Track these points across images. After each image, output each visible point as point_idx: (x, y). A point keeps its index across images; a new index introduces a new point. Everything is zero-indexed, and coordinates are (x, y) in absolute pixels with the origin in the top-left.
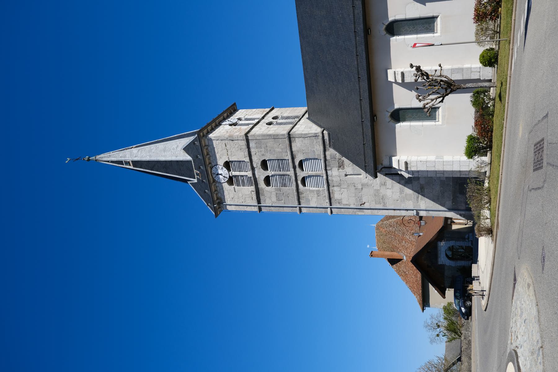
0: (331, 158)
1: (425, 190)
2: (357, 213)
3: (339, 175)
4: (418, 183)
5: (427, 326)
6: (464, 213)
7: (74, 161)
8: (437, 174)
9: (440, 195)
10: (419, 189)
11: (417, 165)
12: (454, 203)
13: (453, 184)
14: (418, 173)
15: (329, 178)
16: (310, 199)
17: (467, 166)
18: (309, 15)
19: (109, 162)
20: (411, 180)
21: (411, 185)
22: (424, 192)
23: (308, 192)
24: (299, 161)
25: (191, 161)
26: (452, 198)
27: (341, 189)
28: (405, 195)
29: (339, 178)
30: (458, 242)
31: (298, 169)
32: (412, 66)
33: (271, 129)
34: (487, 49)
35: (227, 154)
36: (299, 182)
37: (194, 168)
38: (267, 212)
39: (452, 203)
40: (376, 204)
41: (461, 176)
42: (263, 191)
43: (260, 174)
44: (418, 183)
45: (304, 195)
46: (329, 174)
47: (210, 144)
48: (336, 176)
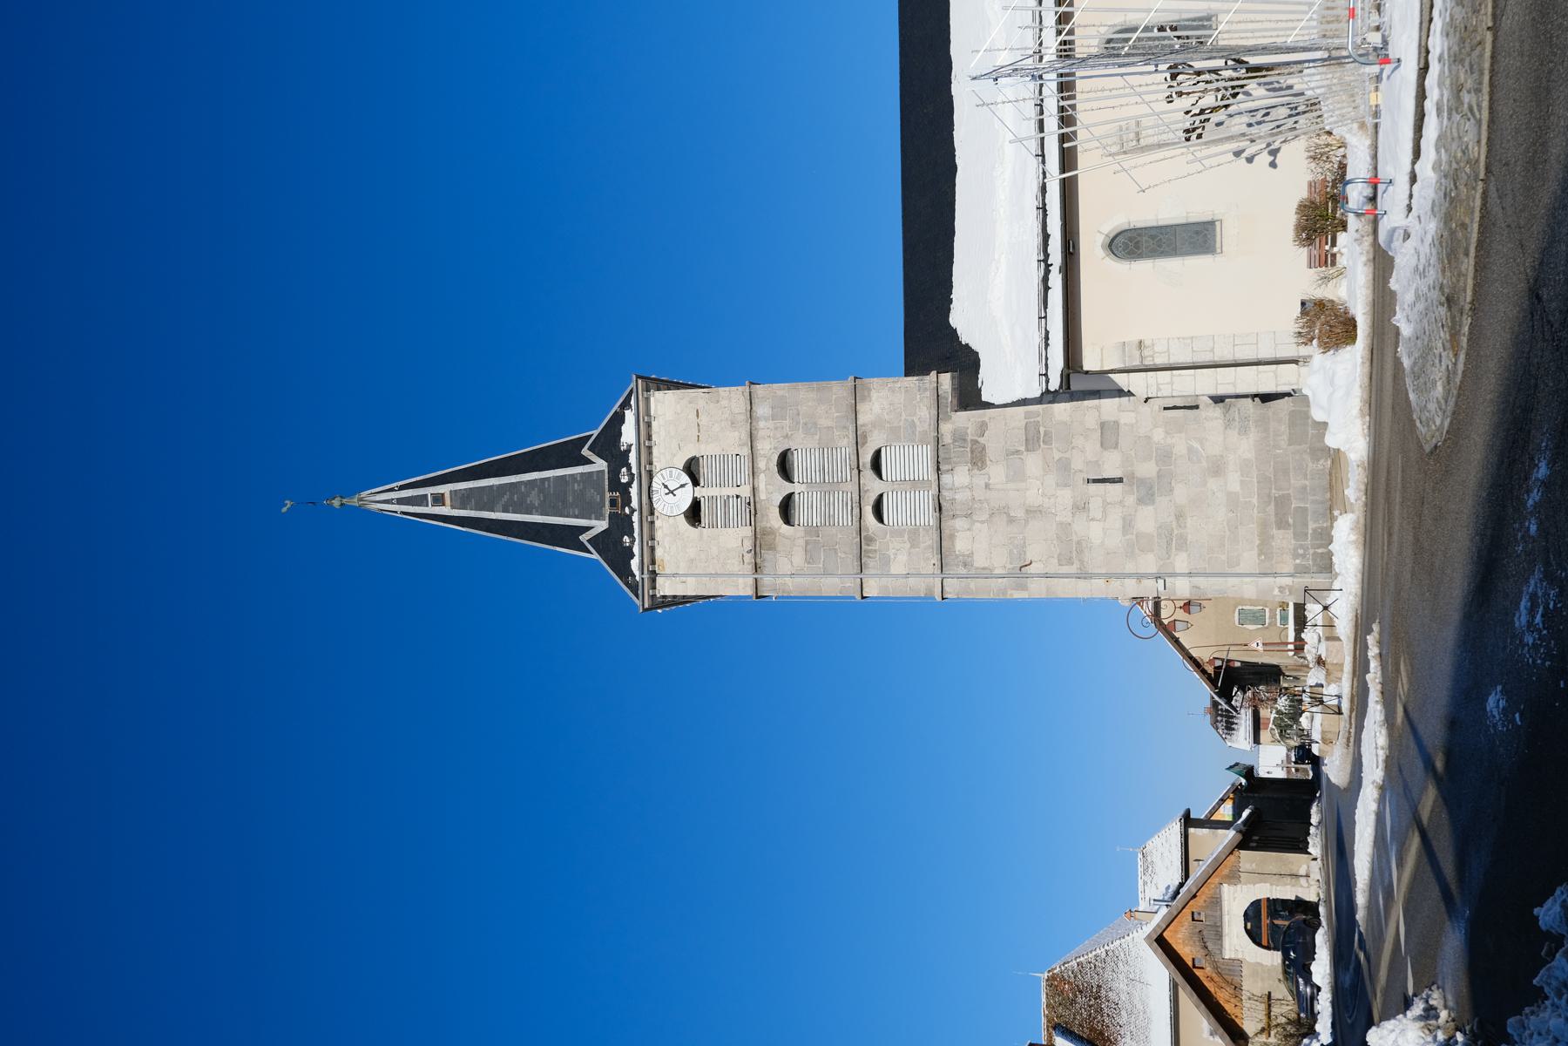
0: (955, 441)
1: (1189, 519)
2: (1009, 592)
4: (1171, 501)
6: (1291, 584)
9: (1228, 533)
10: (1173, 518)
11: (1168, 349)
13: (1259, 502)
14: (1172, 385)
15: (944, 493)
16: (892, 557)
20: (1153, 495)
22: (1185, 527)
24: (874, 450)
26: (1258, 542)
28: (1137, 536)
29: (969, 494)
30: (1278, 888)
31: (868, 473)
35: (699, 432)
36: (868, 510)
37: (607, 487)
39: (1259, 555)
40: (1060, 565)
44: (1171, 501)
46: (946, 484)
47: (659, 413)
48: (962, 487)
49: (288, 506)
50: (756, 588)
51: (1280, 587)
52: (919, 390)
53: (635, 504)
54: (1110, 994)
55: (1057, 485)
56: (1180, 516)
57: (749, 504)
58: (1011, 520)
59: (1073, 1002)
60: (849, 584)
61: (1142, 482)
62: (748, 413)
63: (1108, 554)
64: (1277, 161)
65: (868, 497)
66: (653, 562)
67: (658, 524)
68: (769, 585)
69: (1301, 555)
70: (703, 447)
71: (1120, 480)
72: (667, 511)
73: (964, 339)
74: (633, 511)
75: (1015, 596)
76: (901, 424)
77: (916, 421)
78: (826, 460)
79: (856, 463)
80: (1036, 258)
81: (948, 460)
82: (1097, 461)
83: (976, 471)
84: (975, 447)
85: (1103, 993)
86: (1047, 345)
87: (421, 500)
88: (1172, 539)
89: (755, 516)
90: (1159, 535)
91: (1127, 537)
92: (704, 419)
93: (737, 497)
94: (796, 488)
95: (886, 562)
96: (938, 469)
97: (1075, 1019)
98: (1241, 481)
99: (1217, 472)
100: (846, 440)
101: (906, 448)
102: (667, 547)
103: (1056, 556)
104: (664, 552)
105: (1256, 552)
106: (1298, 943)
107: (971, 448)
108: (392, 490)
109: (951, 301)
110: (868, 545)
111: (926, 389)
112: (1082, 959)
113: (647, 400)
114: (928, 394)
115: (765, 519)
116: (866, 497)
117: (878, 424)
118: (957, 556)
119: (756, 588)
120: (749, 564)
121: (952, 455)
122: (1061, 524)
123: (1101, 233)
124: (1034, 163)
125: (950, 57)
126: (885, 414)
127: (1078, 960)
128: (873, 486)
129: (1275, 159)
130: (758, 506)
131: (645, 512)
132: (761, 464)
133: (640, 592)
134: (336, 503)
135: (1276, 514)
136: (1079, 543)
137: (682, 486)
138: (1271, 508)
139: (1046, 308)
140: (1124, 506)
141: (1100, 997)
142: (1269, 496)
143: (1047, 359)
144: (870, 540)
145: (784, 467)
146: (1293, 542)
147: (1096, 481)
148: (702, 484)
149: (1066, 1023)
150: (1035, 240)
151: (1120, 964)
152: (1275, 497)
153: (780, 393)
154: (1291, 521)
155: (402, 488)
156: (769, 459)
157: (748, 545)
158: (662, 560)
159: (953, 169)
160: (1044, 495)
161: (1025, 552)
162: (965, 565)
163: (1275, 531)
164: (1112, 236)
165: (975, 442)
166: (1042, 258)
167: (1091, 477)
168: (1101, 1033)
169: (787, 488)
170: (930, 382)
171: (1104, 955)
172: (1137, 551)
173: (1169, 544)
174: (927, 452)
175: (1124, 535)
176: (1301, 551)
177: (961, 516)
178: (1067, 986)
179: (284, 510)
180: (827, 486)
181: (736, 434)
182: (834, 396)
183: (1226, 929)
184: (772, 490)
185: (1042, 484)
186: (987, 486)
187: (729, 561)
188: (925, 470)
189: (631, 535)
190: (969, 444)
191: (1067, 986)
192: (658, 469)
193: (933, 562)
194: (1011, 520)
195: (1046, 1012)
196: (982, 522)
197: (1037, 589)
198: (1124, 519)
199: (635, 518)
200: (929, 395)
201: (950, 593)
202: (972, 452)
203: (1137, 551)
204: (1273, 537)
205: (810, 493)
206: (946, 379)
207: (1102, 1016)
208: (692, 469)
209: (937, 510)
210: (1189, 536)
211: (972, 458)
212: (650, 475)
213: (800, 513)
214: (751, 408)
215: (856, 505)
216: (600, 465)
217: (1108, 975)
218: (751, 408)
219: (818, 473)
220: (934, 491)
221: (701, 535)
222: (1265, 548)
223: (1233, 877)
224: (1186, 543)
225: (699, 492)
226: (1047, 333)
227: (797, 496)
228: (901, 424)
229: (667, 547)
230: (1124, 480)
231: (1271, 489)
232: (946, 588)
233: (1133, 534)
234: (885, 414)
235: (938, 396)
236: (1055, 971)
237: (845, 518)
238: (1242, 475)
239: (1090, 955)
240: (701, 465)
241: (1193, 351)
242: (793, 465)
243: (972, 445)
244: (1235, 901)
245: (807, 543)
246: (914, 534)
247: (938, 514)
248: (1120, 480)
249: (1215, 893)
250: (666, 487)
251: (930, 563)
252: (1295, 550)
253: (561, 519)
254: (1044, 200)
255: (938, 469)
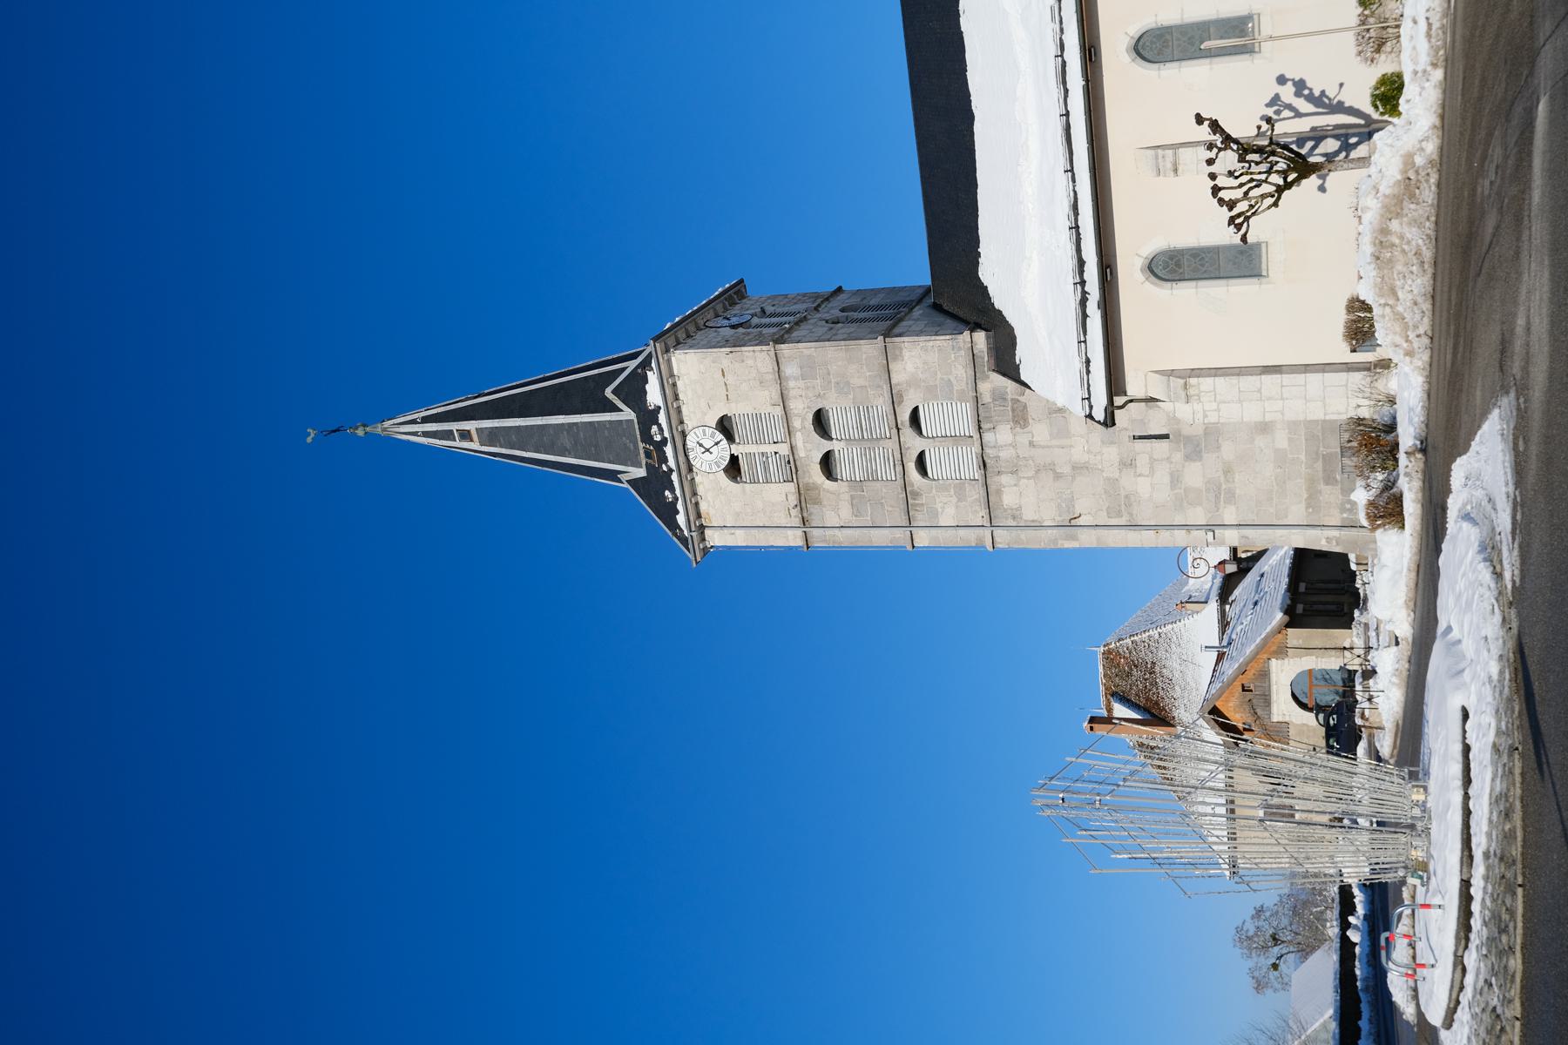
0: (994, 400)
1: (1237, 475)
2: (1060, 542)
3: (1014, 444)
4: (1218, 457)
5: (1246, 940)
7: (326, 435)
8: (1267, 414)
12: (1311, 510)
15: (987, 450)
16: (940, 510)
17: (1341, 386)
18: (939, 35)
19: (418, 436)
20: (1200, 451)
21: (1199, 464)
22: (1234, 481)
23: (934, 491)
25: (633, 420)
26: (1305, 496)
27: (1019, 480)
28: (1185, 490)
30: (1323, 660)
31: (908, 432)
32: (1199, 120)
33: (840, 331)
34: (1253, 915)
38: (825, 547)
39: (1307, 508)
40: (1109, 517)
41: (1328, 418)
42: (817, 492)
43: (809, 446)
45: (922, 500)
48: (1005, 446)
49: (312, 435)
50: (807, 540)
51: (1328, 538)
52: (953, 349)
53: (672, 463)
54: (1164, 671)
55: (1103, 442)
56: (1228, 471)
57: (789, 462)
58: (1058, 476)
59: (1129, 674)
60: (899, 535)
61: (1188, 440)
62: (777, 374)
63: (1157, 507)
64: (1326, 185)
65: (910, 454)
66: (699, 516)
67: (698, 479)
68: (819, 538)
69: (1349, 509)
70: (733, 405)
71: (1166, 437)
72: (705, 468)
73: (997, 306)
74: (671, 471)
75: (1066, 546)
76: (938, 382)
77: (952, 380)
78: (862, 417)
79: (894, 424)
80: (1072, 281)
81: (989, 419)
82: (1142, 420)
83: (1018, 429)
84: (1015, 406)
85: (1157, 669)
86: (1088, 372)
87: (448, 435)
88: (1220, 493)
89: (796, 474)
90: (1208, 490)
91: (1176, 491)
92: (730, 379)
93: (776, 453)
94: (835, 446)
95: (934, 514)
96: (980, 428)
97: (1131, 689)
98: (1289, 438)
99: (1265, 429)
100: (881, 399)
101: (945, 405)
102: (711, 501)
103: (1104, 508)
104: (709, 506)
105: (1303, 505)
106: (1342, 731)
107: (1012, 407)
108: (413, 422)
109: (979, 255)
110: (915, 499)
111: (960, 349)
112: (1136, 638)
113: (669, 361)
114: (963, 353)
115: (807, 475)
116: (908, 454)
117: (914, 382)
118: (1005, 510)
119: (807, 540)
120: (795, 517)
121: (993, 414)
122: (1108, 479)
123: (1139, 256)
124: (1063, 180)
125: (978, 237)
126: (919, 373)
127: (1132, 639)
128: (914, 444)
129: (1324, 182)
130: (798, 463)
131: (684, 471)
132: (796, 423)
133: (690, 546)
134: (360, 432)
135: (1324, 471)
136: (1127, 497)
137: (717, 444)
138: (1319, 465)
139: (1085, 333)
140: (1172, 463)
141: (1154, 672)
142: (1317, 453)
143: (1089, 385)
144: (916, 495)
145: (820, 422)
146: (1340, 497)
147: (1141, 437)
148: (737, 441)
149: (1123, 692)
150: (1070, 263)
151: (1173, 646)
152: (1323, 455)
153: (807, 352)
154: (1338, 477)
155: (425, 420)
156: (804, 419)
157: (793, 500)
158: (708, 514)
159: (970, 118)
160: (1089, 452)
161: (1074, 506)
162: (1014, 518)
163: (1322, 486)
164: (1137, 37)
165: (1015, 401)
166: (1078, 280)
167: (1137, 434)
168: (1157, 703)
169: (826, 446)
170: (964, 342)
171: (1157, 636)
172: (1185, 504)
173: (1217, 497)
174: (967, 409)
175: (1172, 489)
176: (1348, 506)
177: (1007, 473)
178: (1122, 660)
179: (309, 440)
180: (865, 440)
181: (767, 393)
182: (864, 356)
183: (1274, 697)
184: (811, 449)
185: (1087, 441)
186: (1031, 444)
187: (775, 514)
188: (966, 426)
189: (673, 490)
190: (1010, 404)
191: (1122, 660)
192: (690, 428)
193: (981, 514)
194: (1058, 476)
195: (1104, 681)
196: (1029, 478)
197: (1087, 539)
198: (1172, 474)
199: (674, 477)
200: (964, 356)
201: (1000, 543)
202: (1013, 410)
203: (1185, 504)
204: (1320, 492)
205: (850, 449)
206: (980, 337)
207: (1157, 689)
208: (725, 427)
209: (982, 467)
210: (1237, 491)
211: (1014, 416)
212: (684, 435)
213: (842, 468)
214: (779, 369)
215: (898, 463)
216: (628, 414)
217: (1161, 653)
218: (779, 369)
219: (855, 430)
220: (976, 449)
221: (744, 491)
222: (1312, 501)
223: (1281, 653)
224: (1234, 497)
225: (736, 450)
226: (1064, 64)
227: (837, 453)
228: (938, 382)
229: (711, 501)
230: (1171, 436)
231: (1319, 447)
232: (996, 539)
233: (1180, 488)
234: (919, 373)
235: (973, 355)
236: (1111, 647)
237: (888, 472)
238: (1290, 433)
239: (1144, 635)
240: (734, 422)
241: (1240, 391)
242: (829, 419)
243: (1013, 404)
244: (1283, 674)
245: (852, 497)
246: (960, 485)
247: (983, 472)
248: (1166, 437)
249: (1264, 667)
250: (701, 445)
251: (979, 517)
252: (1343, 504)
253: (597, 463)
254: (1076, 220)
255: (980, 428)
